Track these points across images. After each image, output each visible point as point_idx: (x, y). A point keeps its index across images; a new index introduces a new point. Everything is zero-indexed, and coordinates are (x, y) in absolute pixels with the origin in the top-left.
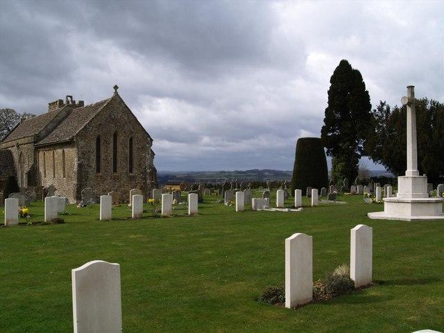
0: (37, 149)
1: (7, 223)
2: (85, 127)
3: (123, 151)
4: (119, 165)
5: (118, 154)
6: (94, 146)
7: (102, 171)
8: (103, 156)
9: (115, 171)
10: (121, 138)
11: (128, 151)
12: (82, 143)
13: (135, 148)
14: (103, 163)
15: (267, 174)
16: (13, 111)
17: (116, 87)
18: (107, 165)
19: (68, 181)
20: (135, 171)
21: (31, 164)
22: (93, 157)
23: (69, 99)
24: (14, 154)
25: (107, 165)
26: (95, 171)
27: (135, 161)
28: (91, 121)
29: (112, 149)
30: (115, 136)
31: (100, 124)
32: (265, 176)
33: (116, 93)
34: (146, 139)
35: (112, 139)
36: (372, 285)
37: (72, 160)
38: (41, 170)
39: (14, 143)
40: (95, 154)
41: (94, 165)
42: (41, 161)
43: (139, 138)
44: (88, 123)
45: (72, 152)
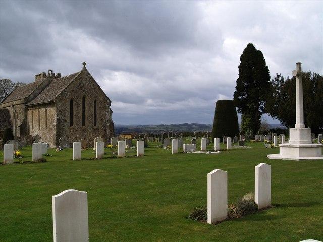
0: (27, 109)
1: (5, 162)
2: (62, 92)
3: (89, 110)
4: (86, 120)
5: (86, 112)
6: (69, 106)
7: (74, 124)
8: (75, 113)
9: (84, 124)
10: (88, 101)
11: (93, 110)
12: (60, 104)
13: (98, 107)
14: (75, 119)
15: (194, 126)
16: (10, 81)
17: (84, 64)
18: (78, 120)
19: (49, 131)
20: (98, 124)
21: (23, 119)
22: (68, 114)
23: (50, 72)
24: (10, 112)
25: (78, 120)
26: (69, 124)
27: (98, 117)
28: (66, 88)
29: (81, 108)
30: (84, 99)
31: (73, 90)
32: (193, 128)
33: (85, 68)
34: (106, 101)
35: (81, 101)
36: (271, 207)
37: (53, 116)
38: (30, 124)
39: (10, 104)
40: (69, 112)
41: (68, 120)
42: (30, 117)
43: (101, 100)
44: (64, 90)
45: (52, 111)
